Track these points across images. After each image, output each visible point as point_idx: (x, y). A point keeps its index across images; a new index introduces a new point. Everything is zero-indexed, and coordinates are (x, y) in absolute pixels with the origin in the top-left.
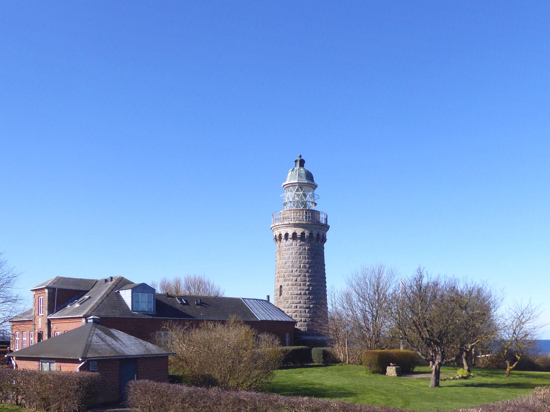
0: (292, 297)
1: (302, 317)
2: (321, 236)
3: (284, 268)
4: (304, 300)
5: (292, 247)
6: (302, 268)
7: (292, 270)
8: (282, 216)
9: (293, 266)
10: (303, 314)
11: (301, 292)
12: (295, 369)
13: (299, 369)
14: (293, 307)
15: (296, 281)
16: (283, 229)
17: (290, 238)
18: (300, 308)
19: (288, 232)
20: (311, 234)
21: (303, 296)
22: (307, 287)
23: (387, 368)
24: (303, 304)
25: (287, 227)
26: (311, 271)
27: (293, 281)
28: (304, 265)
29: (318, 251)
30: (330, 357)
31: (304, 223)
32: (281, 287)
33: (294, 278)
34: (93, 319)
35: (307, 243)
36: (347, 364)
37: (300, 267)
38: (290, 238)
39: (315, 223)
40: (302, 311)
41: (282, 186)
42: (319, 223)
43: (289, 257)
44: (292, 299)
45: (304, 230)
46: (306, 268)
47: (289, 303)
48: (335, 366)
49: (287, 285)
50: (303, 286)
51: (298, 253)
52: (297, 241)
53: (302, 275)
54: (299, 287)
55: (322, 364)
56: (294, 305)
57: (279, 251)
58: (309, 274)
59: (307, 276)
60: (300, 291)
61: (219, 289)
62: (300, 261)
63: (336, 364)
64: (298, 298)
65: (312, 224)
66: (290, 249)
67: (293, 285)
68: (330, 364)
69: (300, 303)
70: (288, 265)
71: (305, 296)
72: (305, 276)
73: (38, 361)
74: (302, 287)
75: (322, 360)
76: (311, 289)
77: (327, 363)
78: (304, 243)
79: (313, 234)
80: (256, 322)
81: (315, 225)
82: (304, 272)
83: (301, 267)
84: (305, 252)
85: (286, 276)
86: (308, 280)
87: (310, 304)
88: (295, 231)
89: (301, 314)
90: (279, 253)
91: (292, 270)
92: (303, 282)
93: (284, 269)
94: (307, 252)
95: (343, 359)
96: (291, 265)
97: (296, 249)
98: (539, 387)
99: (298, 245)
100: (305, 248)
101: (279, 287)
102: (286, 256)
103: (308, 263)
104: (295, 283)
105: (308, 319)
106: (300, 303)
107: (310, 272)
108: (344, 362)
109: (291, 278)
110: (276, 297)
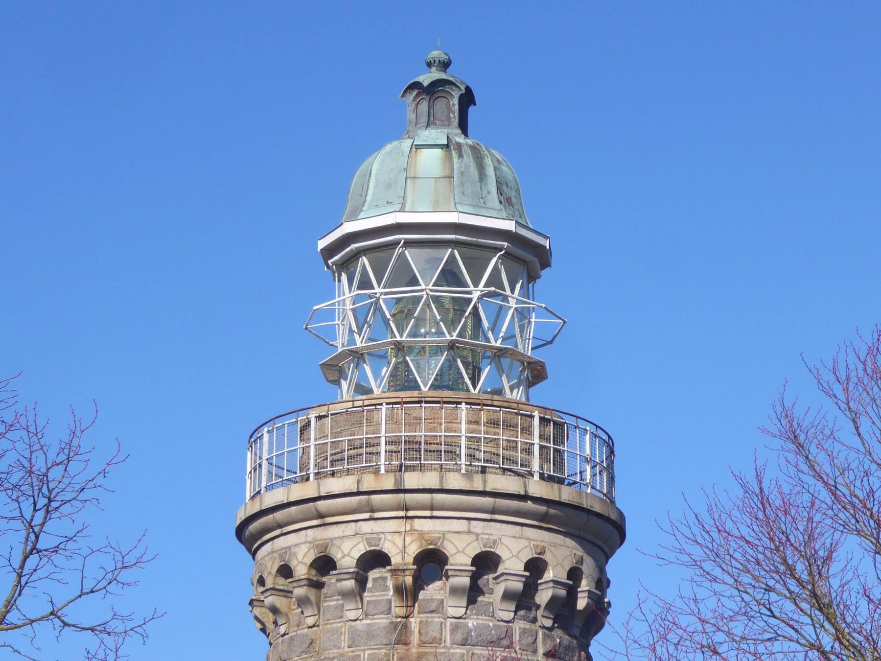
16: (462, 525)
25: (493, 511)
34: (501, 265)
88: (542, 552)
99: (541, 650)
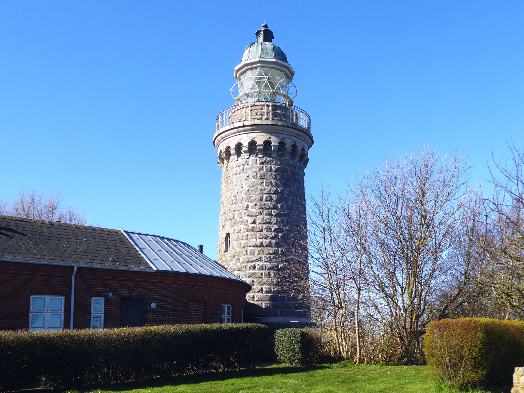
0: (247, 251)
1: (263, 285)
2: (300, 149)
3: (234, 202)
4: (268, 256)
5: (247, 166)
6: (266, 201)
7: (248, 205)
9: (248, 199)
10: (265, 280)
11: (262, 242)
12: (195, 385)
13: (234, 380)
14: (248, 268)
15: (254, 223)
17: (245, 152)
18: (259, 269)
19: (242, 142)
20: (282, 144)
21: (266, 248)
22: (273, 234)
23: (513, 371)
24: (266, 262)
25: (239, 132)
26: (281, 206)
27: (249, 224)
28: (268, 195)
29: (293, 174)
30: (317, 349)
31: (270, 122)
32: (228, 235)
33: (250, 218)
35: (275, 160)
36: (355, 363)
37: (261, 200)
38: (245, 152)
39: (289, 125)
40: (263, 275)
42: (295, 126)
43: (243, 184)
44: (247, 253)
45: (269, 136)
46: (272, 202)
47: (241, 261)
48: (330, 368)
49: (238, 231)
50: (267, 231)
52: (257, 156)
53: (265, 213)
54: (260, 233)
55: (298, 365)
56: (249, 265)
57: (226, 177)
58: (277, 212)
59: (274, 214)
60: (261, 240)
62: (261, 190)
63: (332, 363)
64: (257, 252)
65: (284, 126)
66: (245, 170)
67: (248, 231)
68: (318, 365)
69: (260, 260)
70: (240, 197)
71: (270, 248)
72: (270, 214)
74: (264, 233)
75: (298, 356)
76: (280, 237)
77: (310, 362)
78: (269, 159)
79: (286, 145)
80: (144, 273)
81: (290, 129)
82: (269, 209)
83: (264, 200)
84: (270, 175)
85: (236, 217)
86: (275, 220)
87: (278, 263)
89: (261, 279)
90: (226, 180)
91: (248, 205)
92: (267, 225)
93: (233, 205)
94: (275, 175)
95: (347, 353)
96: (245, 197)
97: (254, 170)
100: (271, 167)
101: (224, 237)
103: (275, 193)
104: (251, 226)
105: (274, 289)
106: (260, 260)
107: (279, 207)
108: (349, 359)
109: (245, 218)
110: (219, 254)
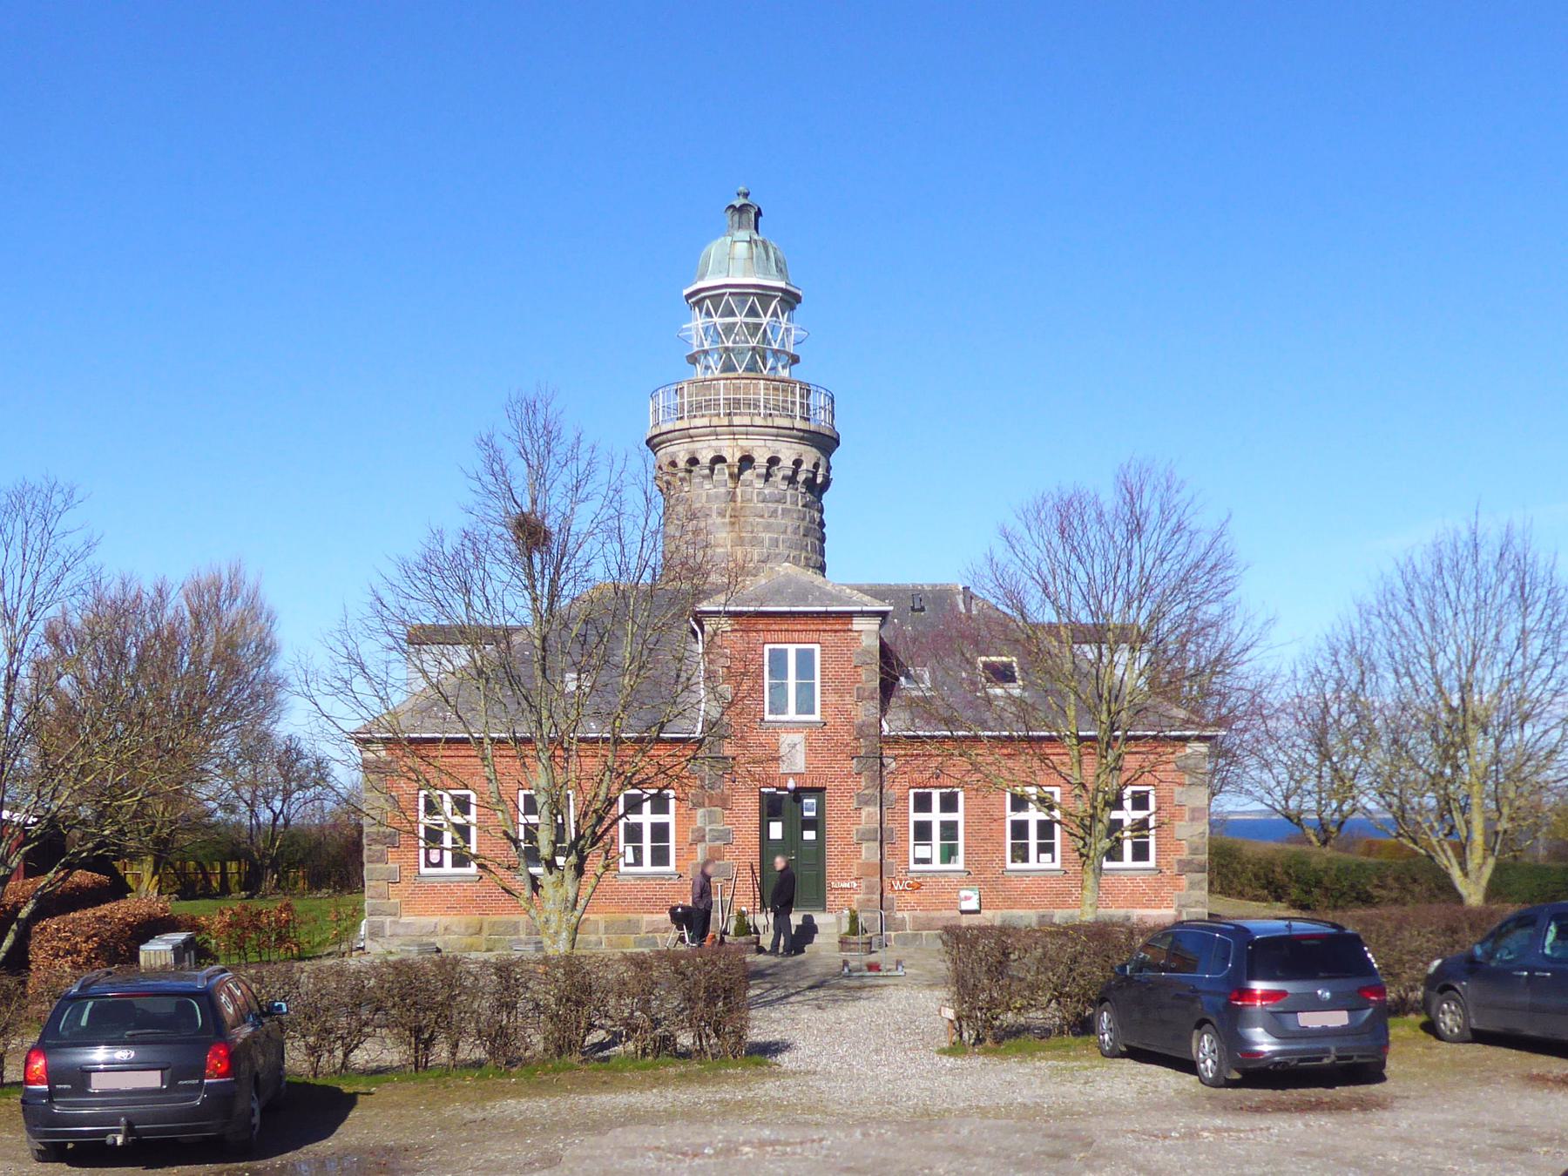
8: (686, 400)
16: (762, 443)
25: (777, 436)
41: (686, 292)
51: (801, 529)
61: (1526, 549)
73: (820, 906)
98: (226, 1063)
99: (800, 504)
102: (766, 536)
